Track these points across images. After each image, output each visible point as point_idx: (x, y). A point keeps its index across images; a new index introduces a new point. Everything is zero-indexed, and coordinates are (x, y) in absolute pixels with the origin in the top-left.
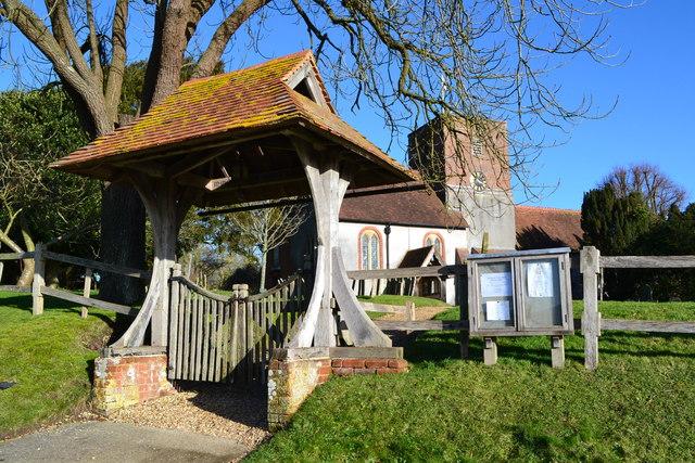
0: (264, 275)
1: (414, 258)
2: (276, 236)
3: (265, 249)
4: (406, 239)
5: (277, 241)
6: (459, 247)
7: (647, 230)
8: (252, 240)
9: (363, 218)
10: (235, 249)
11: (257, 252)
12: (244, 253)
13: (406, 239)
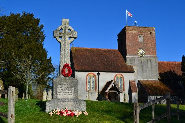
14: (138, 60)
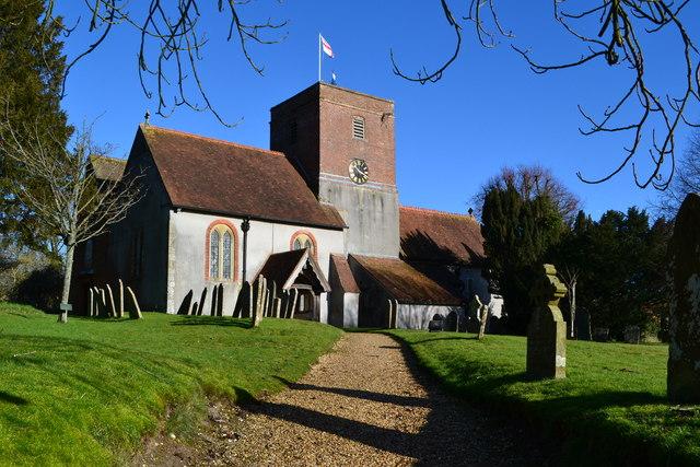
0: (68, 282)
1: (278, 266)
2: (91, 221)
3: (72, 241)
4: (267, 239)
5: (93, 230)
6: (334, 253)
7: (558, 240)
8: (56, 230)
9: (215, 209)
10: (29, 241)
11: (62, 249)
12: (43, 249)
13: (267, 239)
14: (352, 192)
